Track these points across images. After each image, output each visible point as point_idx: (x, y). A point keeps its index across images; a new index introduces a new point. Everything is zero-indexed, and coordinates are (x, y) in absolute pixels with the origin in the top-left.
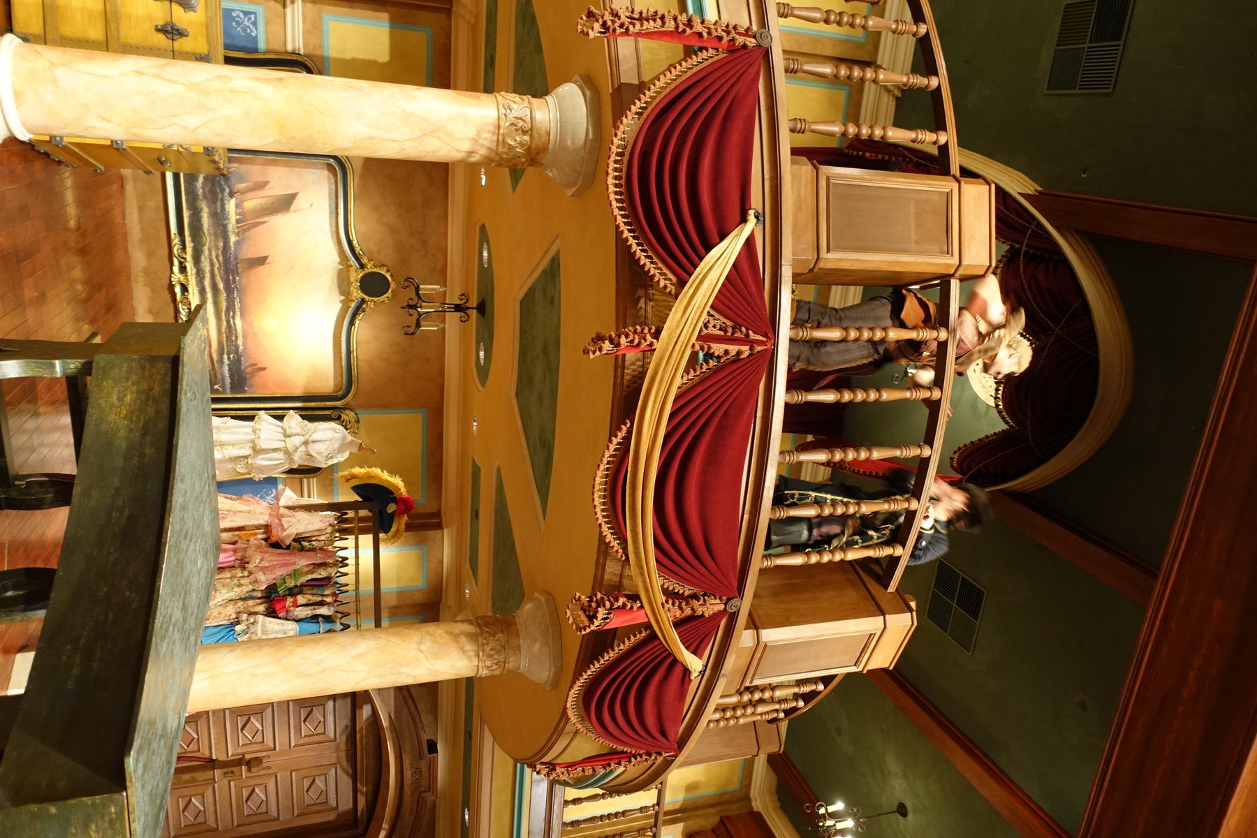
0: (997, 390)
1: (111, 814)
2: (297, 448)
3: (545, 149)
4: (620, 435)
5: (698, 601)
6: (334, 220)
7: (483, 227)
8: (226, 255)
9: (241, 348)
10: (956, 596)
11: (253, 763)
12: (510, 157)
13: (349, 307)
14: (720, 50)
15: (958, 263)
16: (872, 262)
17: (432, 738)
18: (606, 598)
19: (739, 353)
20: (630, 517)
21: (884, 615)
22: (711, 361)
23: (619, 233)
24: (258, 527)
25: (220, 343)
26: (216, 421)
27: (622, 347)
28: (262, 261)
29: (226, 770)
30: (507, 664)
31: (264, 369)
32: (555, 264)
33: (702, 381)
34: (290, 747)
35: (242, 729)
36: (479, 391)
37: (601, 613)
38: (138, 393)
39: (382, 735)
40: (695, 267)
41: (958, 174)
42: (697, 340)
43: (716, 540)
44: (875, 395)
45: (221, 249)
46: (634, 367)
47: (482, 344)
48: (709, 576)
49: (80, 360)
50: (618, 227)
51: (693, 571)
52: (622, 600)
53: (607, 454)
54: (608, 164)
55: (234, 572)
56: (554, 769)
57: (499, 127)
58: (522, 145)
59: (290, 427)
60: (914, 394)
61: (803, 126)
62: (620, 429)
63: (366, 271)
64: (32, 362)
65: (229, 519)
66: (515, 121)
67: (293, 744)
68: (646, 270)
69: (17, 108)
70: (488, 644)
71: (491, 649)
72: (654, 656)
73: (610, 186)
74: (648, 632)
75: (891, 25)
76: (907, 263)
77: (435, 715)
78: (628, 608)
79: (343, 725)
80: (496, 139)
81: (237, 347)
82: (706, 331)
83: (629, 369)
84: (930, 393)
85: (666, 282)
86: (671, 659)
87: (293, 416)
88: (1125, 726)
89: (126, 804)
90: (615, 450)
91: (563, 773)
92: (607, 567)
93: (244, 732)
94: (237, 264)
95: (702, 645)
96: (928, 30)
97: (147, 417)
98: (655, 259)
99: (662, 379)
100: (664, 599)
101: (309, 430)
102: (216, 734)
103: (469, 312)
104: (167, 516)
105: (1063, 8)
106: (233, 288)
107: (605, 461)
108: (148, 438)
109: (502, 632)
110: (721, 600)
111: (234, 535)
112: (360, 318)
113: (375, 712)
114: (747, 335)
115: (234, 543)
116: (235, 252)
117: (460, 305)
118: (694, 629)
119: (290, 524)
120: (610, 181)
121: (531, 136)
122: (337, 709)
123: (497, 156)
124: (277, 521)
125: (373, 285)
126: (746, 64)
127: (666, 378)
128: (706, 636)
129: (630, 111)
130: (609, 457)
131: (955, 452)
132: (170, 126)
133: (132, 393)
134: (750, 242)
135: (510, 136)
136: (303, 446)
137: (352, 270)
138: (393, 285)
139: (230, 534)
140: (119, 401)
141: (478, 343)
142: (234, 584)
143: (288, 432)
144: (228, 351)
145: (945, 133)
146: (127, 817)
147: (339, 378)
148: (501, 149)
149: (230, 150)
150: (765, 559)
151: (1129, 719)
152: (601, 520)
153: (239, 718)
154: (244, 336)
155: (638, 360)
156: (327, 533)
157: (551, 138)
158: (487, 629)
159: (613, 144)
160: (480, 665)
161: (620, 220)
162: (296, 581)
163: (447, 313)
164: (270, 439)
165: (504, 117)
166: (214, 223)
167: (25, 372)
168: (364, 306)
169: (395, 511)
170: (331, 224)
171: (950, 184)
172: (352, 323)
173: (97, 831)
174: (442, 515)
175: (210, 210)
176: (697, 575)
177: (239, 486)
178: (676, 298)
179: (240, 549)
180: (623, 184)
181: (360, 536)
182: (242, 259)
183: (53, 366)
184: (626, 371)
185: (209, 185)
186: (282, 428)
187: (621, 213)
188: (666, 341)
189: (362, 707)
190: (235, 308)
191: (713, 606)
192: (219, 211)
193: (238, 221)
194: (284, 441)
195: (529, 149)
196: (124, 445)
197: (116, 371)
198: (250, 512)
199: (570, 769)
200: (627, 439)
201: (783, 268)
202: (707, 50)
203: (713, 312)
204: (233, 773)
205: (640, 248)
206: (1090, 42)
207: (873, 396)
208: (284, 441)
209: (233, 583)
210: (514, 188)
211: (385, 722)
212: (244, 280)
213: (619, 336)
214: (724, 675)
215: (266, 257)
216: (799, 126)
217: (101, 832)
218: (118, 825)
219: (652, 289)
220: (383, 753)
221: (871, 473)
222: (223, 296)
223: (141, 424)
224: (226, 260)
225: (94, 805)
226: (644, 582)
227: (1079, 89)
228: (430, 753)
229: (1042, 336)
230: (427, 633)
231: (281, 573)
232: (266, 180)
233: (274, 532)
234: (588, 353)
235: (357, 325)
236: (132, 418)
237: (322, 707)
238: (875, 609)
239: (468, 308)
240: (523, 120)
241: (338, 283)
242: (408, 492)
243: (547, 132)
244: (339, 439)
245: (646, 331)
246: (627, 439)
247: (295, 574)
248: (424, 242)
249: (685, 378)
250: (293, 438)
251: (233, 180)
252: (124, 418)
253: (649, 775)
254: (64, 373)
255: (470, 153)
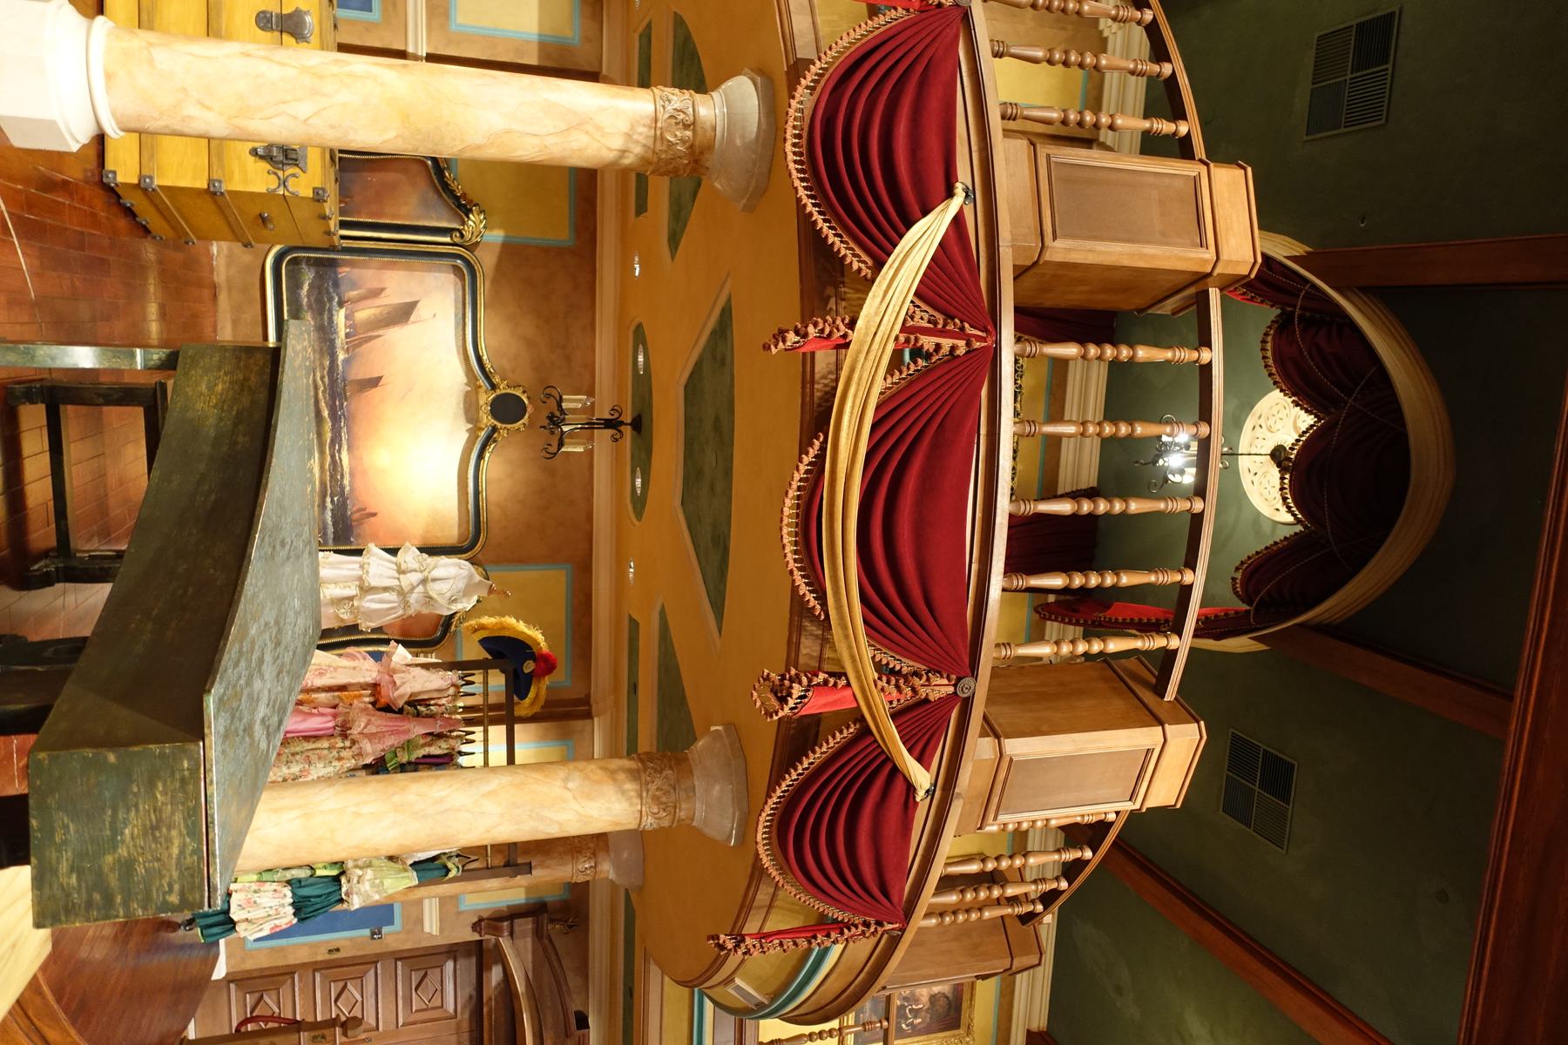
0: (1282, 478)
1: (183, 770)
2: (413, 588)
3: (709, 147)
4: (812, 452)
5: (920, 679)
6: (461, 333)
7: (639, 327)
8: (333, 376)
9: (347, 488)
10: (1259, 774)
11: (349, 1024)
12: (669, 156)
13: (478, 436)
14: (912, 10)
15: (1215, 258)
16: (1110, 253)
17: (581, 1009)
18: (802, 674)
19: (953, 348)
20: (828, 559)
21: (1162, 724)
22: (919, 360)
23: (801, 207)
24: (364, 686)
25: (323, 483)
26: (321, 554)
27: (811, 337)
28: (375, 382)
29: (313, 1034)
30: (678, 810)
31: (374, 515)
32: (726, 313)
33: (911, 383)
34: (397, 1027)
35: (336, 1000)
36: (634, 525)
37: (797, 690)
38: (231, 382)
39: (516, 1007)
40: (895, 246)
41: (1204, 157)
42: (901, 331)
43: (940, 594)
44: (1127, 428)
45: (327, 369)
46: (826, 382)
47: (638, 469)
48: (933, 645)
49: (165, 350)
50: (799, 200)
51: (910, 636)
52: (822, 676)
53: (797, 476)
54: (785, 129)
55: (332, 741)
56: (743, 941)
57: (656, 121)
58: (683, 141)
59: (405, 562)
60: (1178, 353)
61: (1015, 111)
62: (811, 445)
63: (498, 392)
64: (109, 351)
65: (328, 675)
66: (675, 114)
67: (400, 1023)
68: (835, 250)
69: (107, 92)
70: (653, 782)
71: (657, 789)
72: (868, 760)
73: (788, 153)
74: (858, 726)
75: (1111, 10)
76: (1153, 257)
77: (586, 977)
78: (830, 685)
79: (466, 995)
80: (653, 134)
81: (342, 488)
82: (912, 323)
83: (819, 383)
84: (1196, 429)
85: (860, 264)
86: (887, 769)
87: (409, 549)
88: (1500, 886)
89: (202, 758)
90: (807, 472)
91: (754, 946)
92: (801, 646)
93: (338, 1004)
94: (345, 386)
95: (928, 752)
96: (1154, 16)
97: (241, 407)
98: (846, 238)
99: (860, 379)
100: (876, 675)
101: (428, 565)
102: (302, 1006)
103: (622, 428)
104: (262, 491)
105: (1315, 42)
106: (340, 416)
107: (795, 485)
108: (241, 428)
109: (671, 768)
110: (949, 680)
111: (333, 696)
112: (490, 450)
113: (507, 977)
114: (962, 329)
115: (335, 707)
116: (343, 372)
117: (611, 420)
118: (918, 720)
119: (404, 680)
120: (789, 148)
121: (694, 131)
122: (458, 972)
123: (655, 156)
124: (387, 677)
125: (506, 409)
126: (942, 24)
127: (865, 376)
128: (932, 735)
129: (809, 71)
130: (800, 481)
131: (1237, 569)
132: (276, 116)
133: (224, 382)
134: (958, 221)
135: (670, 131)
136: (421, 586)
137: (482, 391)
138: (530, 409)
139: (329, 695)
140: (209, 391)
141: (633, 472)
142: (333, 757)
143: (403, 566)
144: (331, 493)
145: (1185, 122)
146: (202, 776)
147: (464, 525)
148: (659, 147)
149: (341, 151)
150: (1003, 647)
151: (1505, 876)
152: (792, 565)
153: (332, 984)
154: (352, 474)
155: (830, 373)
156: (449, 696)
157: (717, 132)
158: (652, 765)
159: (790, 107)
160: (644, 809)
161: (802, 193)
162: (409, 754)
163: (596, 431)
164: (381, 575)
165: (662, 110)
166: (319, 339)
167: (100, 363)
168: (495, 435)
169: (533, 671)
170: (456, 338)
171: (1197, 166)
172: (481, 456)
173: (164, 793)
174: (592, 700)
175: (315, 322)
176: (915, 640)
177: (340, 638)
178: (873, 281)
179: (341, 713)
180: (809, 573)
181: (490, 728)
182: (352, 381)
183: (133, 356)
184: (816, 386)
185: (316, 292)
186: (396, 564)
187: (803, 184)
188: (863, 332)
189: (491, 969)
190: (341, 440)
191: (940, 688)
192: (326, 324)
193: (347, 335)
194: (399, 579)
195: (692, 146)
196: (212, 433)
197: (207, 360)
198: (354, 668)
199: (763, 941)
200: (821, 457)
201: (1000, 249)
202: (896, 9)
203: (918, 302)
204: (323, 1037)
205: (828, 224)
206: (1352, 73)
207: (1124, 429)
208: (399, 579)
209: (332, 755)
210: (673, 257)
211: (520, 987)
212: (353, 407)
213: (806, 327)
214: (959, 794)
215: (379, 378)
216: (1009, 111)
217: (170, 794)
218: (191, 787)
219: (844, 287)
220: (518, 1035)
221: (1132, 619)
222: (328, 425)
223: (234, 413)
224: (333, 382)
225: (162, 756)
226: (850, 647)
227: (1345, 127)
228: (578, 1028)
229: (1333, 410)
230: (576, 768)
231: (390, 743)
232: (382, 286)
233: (384, 691)
234: (770, 346)
235: (486, 459)
236: (223, 407)
237: (439, 970)
238: (1149, 718)
239: (622, 423)
240: (684, 113)
241: (465, 408)
242: (550, 646)
243: (712, 127)
244: (464, 578)
245: (839, 322)
246: (821, 457)
247: (408, 745)
248: (568, 358)
249: (889, 380)
250: (408, 575)
251: (343, 288)
252: (214, 407)
253: (868, 973)
254: (145, 365)
255: (624, 152)
